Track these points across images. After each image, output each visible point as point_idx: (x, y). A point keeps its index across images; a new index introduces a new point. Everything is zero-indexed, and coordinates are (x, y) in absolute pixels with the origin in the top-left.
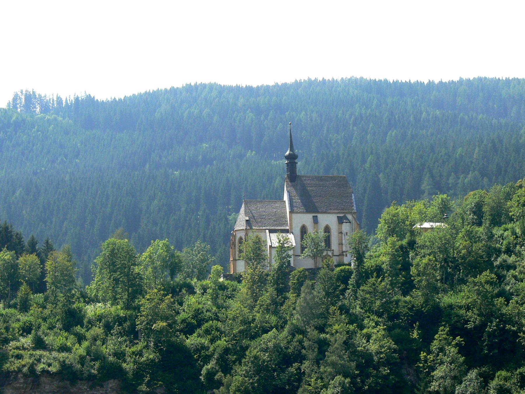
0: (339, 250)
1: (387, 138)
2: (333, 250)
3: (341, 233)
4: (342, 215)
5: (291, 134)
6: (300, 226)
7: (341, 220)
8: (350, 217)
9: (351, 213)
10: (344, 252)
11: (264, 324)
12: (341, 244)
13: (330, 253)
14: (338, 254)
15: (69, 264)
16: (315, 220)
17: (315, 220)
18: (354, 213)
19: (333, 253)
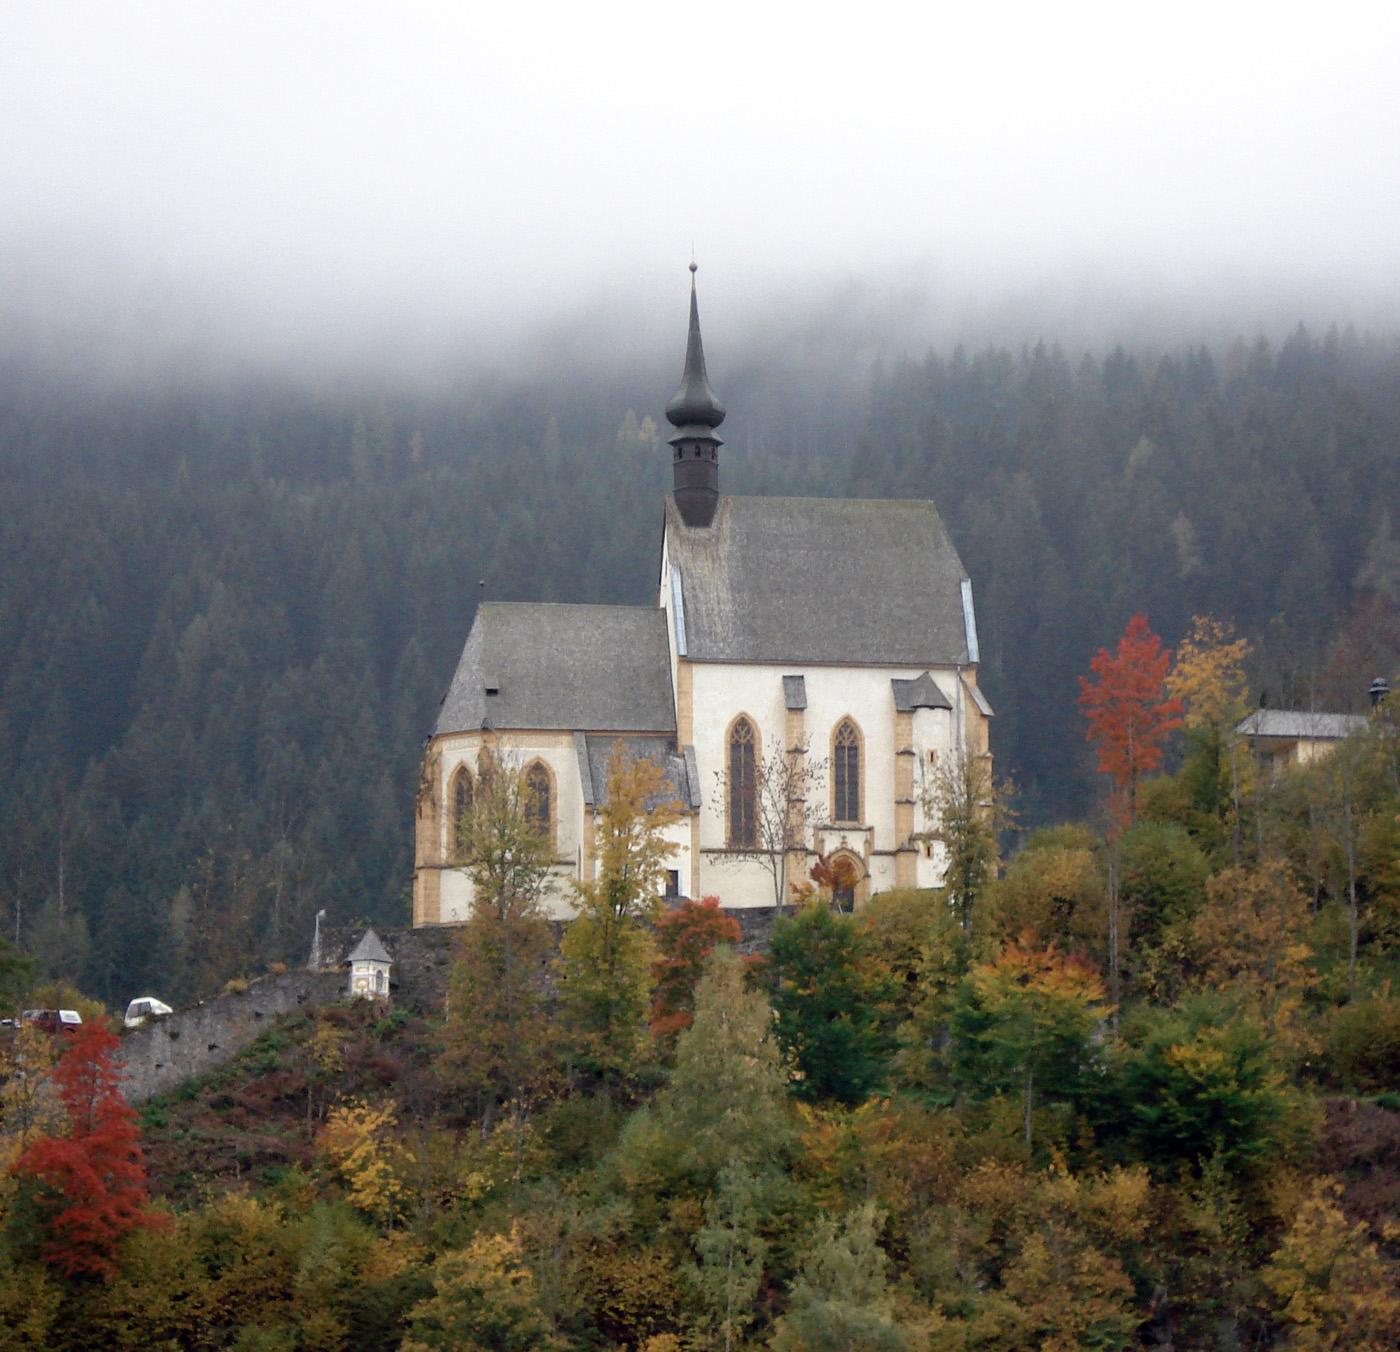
0: (898, 830)
1: (766, 800)
2: (870, 829)
3: (909, 753)
4: (911, 675)
5: (693, 284)
6: (726, 719)
7: (909, 702)
8: (947, 684)
9: (949, 666)
10: (919, 836)
11: (1306, 791)
12: (905, 803)
13: (856, 842)
14: (892, 847)
15: (629, 1234)
16: (795, 704)
17: (795, 704)
18: (968, 666)
19: (868, 843)
